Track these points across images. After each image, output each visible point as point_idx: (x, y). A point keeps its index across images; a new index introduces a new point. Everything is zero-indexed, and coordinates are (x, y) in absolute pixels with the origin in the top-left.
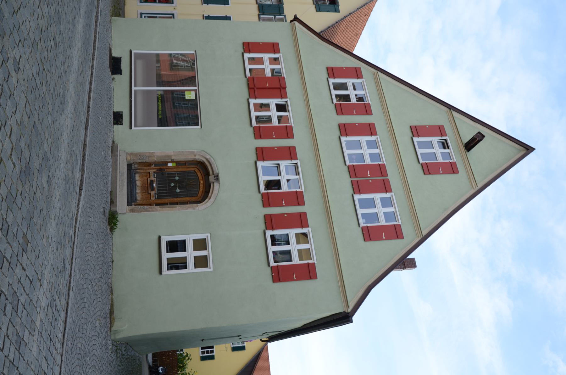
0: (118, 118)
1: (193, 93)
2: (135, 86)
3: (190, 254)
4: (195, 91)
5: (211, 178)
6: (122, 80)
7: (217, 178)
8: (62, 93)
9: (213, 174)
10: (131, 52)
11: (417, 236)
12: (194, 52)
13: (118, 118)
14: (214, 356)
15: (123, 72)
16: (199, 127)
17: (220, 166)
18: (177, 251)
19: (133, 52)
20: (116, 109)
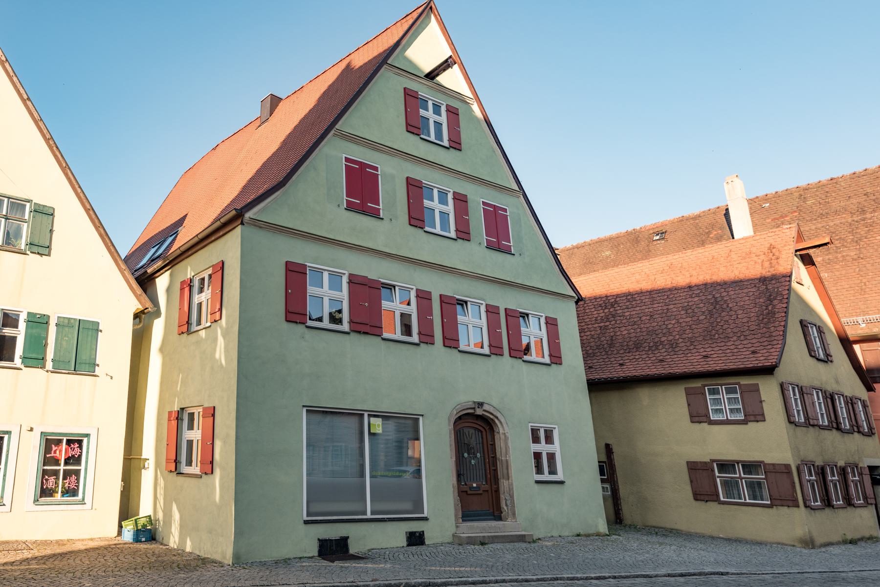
0: (416, 539)
1: (372, 420)
2: (365, 513)
3: (543, 448)
4: (369, 416)
5: (479, 412)
6: (362, 538)
7: (481, 405)
8: (757, 490)
9: (474, 408)
10: (306, 522)
11: (518, 197)
12: (305, 409)
13: (416, 539)
14: (64, 324)
15: (344, 534)
16: (421, 418)
17: (465, 397)
18: (307, 458)
19: (305, 518)
20: (402, 541)
